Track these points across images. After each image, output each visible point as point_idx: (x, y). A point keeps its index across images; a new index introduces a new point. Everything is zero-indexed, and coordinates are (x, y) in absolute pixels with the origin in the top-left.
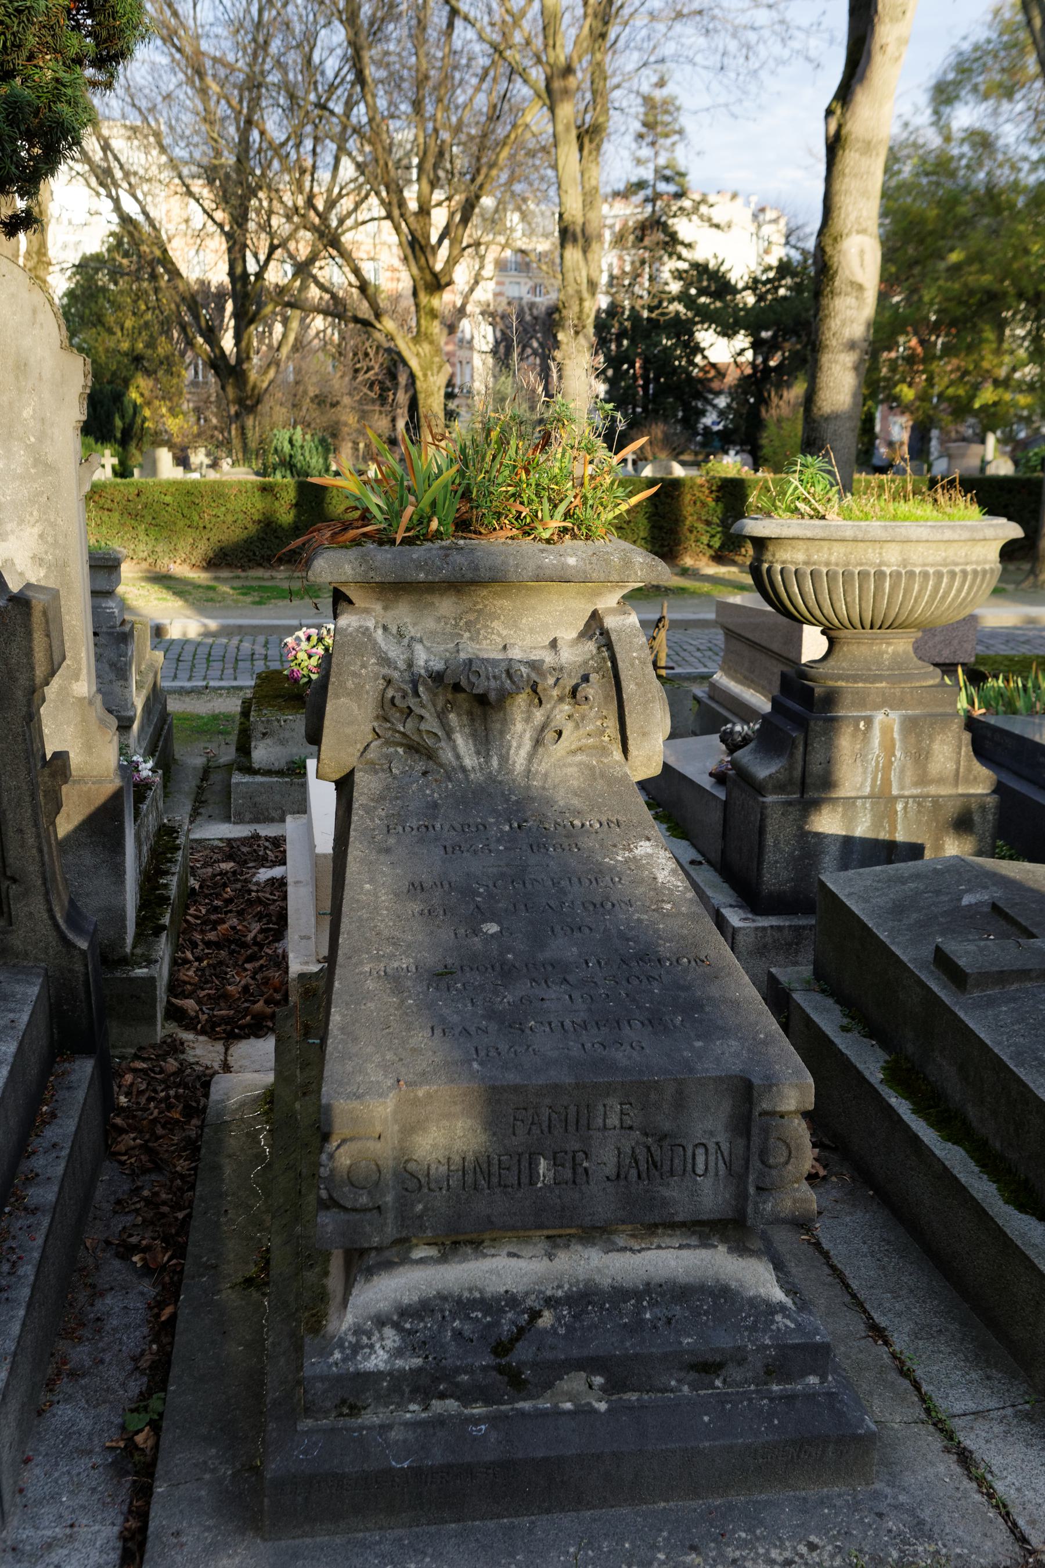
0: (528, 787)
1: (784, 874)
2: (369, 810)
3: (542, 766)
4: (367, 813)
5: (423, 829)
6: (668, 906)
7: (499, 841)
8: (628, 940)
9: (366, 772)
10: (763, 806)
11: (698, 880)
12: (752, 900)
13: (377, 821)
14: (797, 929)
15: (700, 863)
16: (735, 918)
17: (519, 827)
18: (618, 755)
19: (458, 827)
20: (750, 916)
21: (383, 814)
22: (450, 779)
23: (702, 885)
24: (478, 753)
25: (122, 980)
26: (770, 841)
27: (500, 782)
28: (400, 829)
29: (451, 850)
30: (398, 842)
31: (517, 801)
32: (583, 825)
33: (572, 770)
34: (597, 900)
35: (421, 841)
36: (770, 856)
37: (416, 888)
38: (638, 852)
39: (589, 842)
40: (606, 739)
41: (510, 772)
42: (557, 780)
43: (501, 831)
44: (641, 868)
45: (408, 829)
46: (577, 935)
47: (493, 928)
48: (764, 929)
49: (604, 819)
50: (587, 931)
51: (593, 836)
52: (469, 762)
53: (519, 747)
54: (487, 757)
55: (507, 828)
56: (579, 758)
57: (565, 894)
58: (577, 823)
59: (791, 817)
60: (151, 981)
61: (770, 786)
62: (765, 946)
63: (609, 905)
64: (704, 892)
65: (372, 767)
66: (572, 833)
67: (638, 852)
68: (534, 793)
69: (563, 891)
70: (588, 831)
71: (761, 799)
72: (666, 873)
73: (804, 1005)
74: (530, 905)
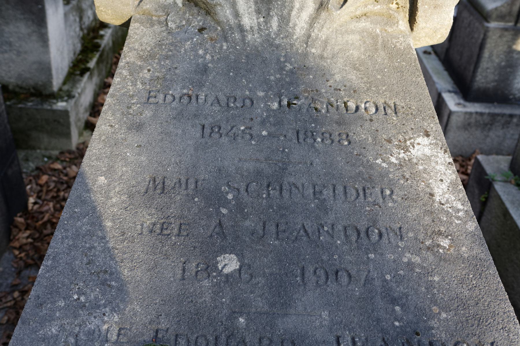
0: (306, 55)
1: (491, 77)
2: (133, 70)
3: (322, 32)
4: (131, 74)
5: (185, 100)
6: (445, 243)
7: (263, 123)
8: (394, 301)
9: (142, 23)
10: (487, 30)
11: (428, 66)
12: (465, 90)
13: (140, 86)
14: (493, 116)
15: (430, 53)
16: (452, 102)
17: (289, 104)
18: (403, 24)
19: (223, 99)
20: (462, 101)
21: (148, 76)
22: (226, 39)
23: (430, 71)
24: (258, 12)
25: (48, 110)
26: (486, 54)
27: (278, 47)
28: (161, 96)
29: (211, 131)
30: (155, 116)
31: (292, 72)
32: (357, 108)
33: (354, 38)
34: (362, 225)
35: (179, 116)
36: (484, 64)
37: (158, 186)
38: (416, 152)
39: (361, 134)
40: (394, 6)
41: (289, 35)
42: (337, 48)
43: (268, 109)
44: (415, 175)
45: (169, 98)
46: (332, 287)
47: (229, 264)
48: (471, 114)
49: (381, 102)
50: (344, 279)
51: (367, 125)
52: (248, 20)
53: (301, 9)
54: (267, 17)
55: (275, 106)
56: (363, 24)
57: (326, 211)
58: (352, 105)
59: (505, 39)
60: (65, 113)
61: (494, 16)
62: (469, 124)
63: (375, 237)
64: (431, 77)
65: (149, 20)
66: (347, 117)
67: (416, 152)
68: (311, 62)
69: (323, 207)
70: (361, 118)
71: (487, 24)
72: (444, 186)
73: (504, 198)
74: (282, 227)
